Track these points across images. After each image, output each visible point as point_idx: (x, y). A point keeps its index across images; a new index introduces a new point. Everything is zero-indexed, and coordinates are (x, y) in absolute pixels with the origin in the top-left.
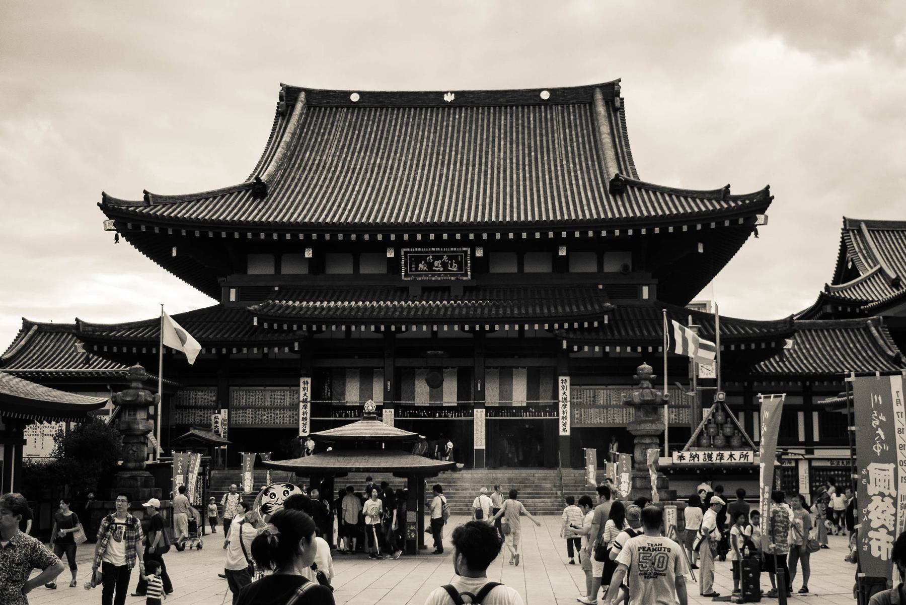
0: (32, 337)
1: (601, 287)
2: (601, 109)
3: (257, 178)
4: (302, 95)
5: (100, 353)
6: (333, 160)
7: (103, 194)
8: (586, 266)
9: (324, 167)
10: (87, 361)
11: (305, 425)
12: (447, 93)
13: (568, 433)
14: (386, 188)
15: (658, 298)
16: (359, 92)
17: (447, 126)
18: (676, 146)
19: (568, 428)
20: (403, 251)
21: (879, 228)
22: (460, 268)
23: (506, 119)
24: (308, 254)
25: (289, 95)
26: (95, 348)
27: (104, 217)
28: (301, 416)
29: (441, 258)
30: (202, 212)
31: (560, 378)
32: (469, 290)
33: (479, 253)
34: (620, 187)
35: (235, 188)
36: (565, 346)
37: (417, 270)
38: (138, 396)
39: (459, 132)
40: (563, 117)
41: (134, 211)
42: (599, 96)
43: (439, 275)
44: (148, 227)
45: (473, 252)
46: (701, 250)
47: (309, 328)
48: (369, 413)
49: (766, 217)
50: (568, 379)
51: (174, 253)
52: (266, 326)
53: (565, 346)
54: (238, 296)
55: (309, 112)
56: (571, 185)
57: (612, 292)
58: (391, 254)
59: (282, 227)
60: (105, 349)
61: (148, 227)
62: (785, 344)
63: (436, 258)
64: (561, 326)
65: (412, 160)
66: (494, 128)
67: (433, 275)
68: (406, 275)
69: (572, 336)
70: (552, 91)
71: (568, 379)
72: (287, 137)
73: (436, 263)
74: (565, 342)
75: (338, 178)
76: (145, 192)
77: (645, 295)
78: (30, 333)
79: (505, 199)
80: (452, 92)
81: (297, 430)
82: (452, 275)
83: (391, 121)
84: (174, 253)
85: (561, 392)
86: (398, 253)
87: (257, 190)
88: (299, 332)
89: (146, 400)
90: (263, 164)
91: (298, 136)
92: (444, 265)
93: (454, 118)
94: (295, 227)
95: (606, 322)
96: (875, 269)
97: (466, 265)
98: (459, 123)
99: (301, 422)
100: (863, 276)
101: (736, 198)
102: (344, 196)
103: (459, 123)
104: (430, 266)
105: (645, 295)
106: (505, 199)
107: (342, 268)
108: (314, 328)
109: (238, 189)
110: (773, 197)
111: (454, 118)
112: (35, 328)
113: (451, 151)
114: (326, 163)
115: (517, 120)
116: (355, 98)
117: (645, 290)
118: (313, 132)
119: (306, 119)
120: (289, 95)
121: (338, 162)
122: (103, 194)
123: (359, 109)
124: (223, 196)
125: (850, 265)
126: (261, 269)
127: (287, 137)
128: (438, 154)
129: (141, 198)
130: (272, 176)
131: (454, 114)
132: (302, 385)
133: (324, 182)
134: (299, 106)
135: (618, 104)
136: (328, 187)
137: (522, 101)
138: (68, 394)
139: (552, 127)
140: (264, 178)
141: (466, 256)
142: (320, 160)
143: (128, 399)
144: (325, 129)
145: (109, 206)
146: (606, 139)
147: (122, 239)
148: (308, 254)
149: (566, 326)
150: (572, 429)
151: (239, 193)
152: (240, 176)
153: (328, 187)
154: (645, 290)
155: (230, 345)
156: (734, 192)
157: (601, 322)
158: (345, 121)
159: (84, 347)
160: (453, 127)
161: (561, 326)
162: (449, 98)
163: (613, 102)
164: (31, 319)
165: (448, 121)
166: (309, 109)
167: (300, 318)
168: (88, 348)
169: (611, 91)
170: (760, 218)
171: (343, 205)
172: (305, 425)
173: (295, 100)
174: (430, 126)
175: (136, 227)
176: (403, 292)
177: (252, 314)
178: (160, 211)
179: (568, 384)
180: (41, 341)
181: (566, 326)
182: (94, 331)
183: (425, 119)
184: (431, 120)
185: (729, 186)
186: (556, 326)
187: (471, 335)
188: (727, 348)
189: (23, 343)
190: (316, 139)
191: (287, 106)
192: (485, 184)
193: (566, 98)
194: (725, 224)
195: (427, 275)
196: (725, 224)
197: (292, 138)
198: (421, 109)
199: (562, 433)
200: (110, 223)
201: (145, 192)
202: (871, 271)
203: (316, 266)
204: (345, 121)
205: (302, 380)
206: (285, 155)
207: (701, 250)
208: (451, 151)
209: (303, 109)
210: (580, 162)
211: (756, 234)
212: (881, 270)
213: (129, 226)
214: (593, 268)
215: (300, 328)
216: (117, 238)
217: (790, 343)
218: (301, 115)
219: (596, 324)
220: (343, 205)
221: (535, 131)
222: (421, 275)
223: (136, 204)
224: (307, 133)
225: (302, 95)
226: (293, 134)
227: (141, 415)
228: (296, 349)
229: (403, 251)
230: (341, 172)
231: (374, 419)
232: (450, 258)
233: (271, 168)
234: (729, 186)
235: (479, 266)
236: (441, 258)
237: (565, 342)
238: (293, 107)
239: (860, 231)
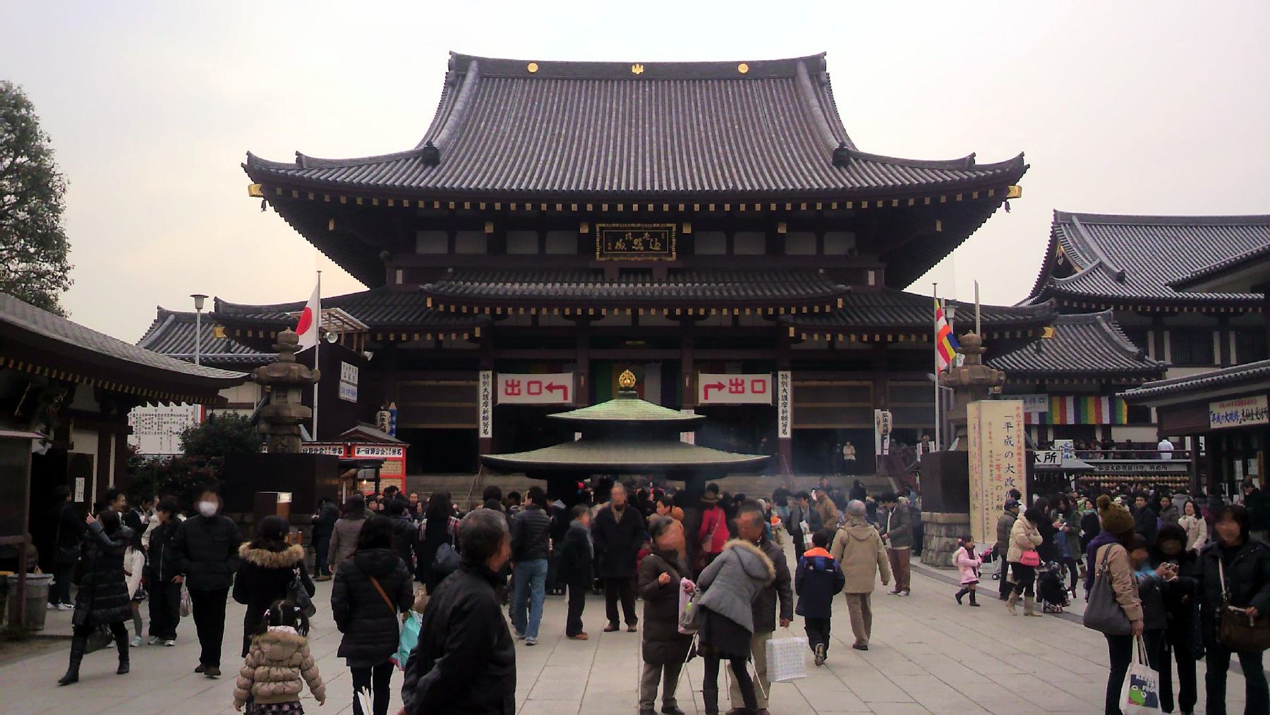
0: (168, 327)
1: (821, 271)
2: (806, 81)
3: (429, 143)
4: (474, 64)
5: (244, 341)
6: (511, 131)
7: (248, 154)
8: (802, 247)
9: (502, 137)
10: (228, 349)
11: (486, 425)
12: (635, 64)
13: (788, 436)
14: (576, 159)
15: (887, 283)
16: (537, 63)
17: (637, 99)
18: (893, 121)
19: (788, 430)
20: (598, 226)
21: (1091, 221)
22: (663, 248)
23: (701, 93)
24: (489, 229)
25: (459, 65)
26: (238, 333)
27: (249, 181)
28: (481, 415)
29: (641, 235)
30: (366, 178)
31: (780, 373)
32: (673, 273)
33: (687, 230)
34: (844, 156)
35: (402, 154)
36: (792, 335)
37: (613, 249)
38: (290, 370)
39: (650, 105)
40: (764, 91)
41: (286, 174)
42: (802, 70)
43: (639, 255)
44: (302, 195)
45: (680, 229)
46: (939, 228)
47: (493, 311)
48: (627, 389)
49: (1020, 188)
50: (789, 373)
51: (331, 227)
52: (441, 308)
53: (792, 335)
54: (405, 279)
55: (478, 82)
56: (787, 158)
57: (837, 274)
58: (584, 230)
59: (460, 195)
60: (250, 334)
61: (302, 195)
62: (1044, 332)
63: (635, 235)
64: (788, 311)
65: (602, 132)
66: (690, 102)
67: (633, 256)
68: (601, 255)
69: (800, 321)
70: (750, 64)
71: (789, 373)
72: (459, 106)
73: (636, 241)
74: (792, 329)
75: (520, 148)
76: (297, 153)
77: (871, 281)
78: (167, 323)
79: (714, 171)
80: (640, 64)
81: (477, 431)
82: (654, 255)
83: (573, 94)
84: (331, 227)
85: (781, 389)
86: (592, 230)
87: (428, 155)
88: (481, 316)
89: (301, 377)
90: (436, 127)
91: (471, 106)
92: (646, 243)
93: (644, 91)
94: (475, 195)
95: (840, 306)
96: (1095, 264)
97: (671, 243)
98: (650, 97)
99: (482, 422)
100: (1080, 272)
101: (983, 168)
102: (529, 165)
103: (650, 97)
104: (629, 244)
105: (871, 281)
106: (714, 171)
107: (523, 245)
108: (499, 311)
109: (406, 156)
110: (1029, 166)
111: (644, 91)
112: (172, 317)
113: (644, 123)
114: (504, 133)
115: (714, 94)
116: (533, 68)
117: (871, 275)
118: (487, 102)
119: (479, 89)
120: (459, 65)
121: (518, 133)
122: (248, 154)
123: (538, 80)
124: (388, 163)
125: (1060, 262)
126: (431, 246)
127: (459, 106)
128: (630, 125)
129: (292, 160)
130: (446, 143)
131: (644, 87)
132: (482, 380)
133: (504, 152)
134: (471, 76)
135: (824, 79)
136: (509, 157)
137: (721, 74)
138: (192, 373)
139: (754, 102)
140: (436, 144)
141: (671, 233)
142: (497, 132)
143: (276, 375)
144: (501, 100)
145: (259, 171)
146: (817, 110)
147: (270, 209)
148: (489, 229)
149: (793, 311)
150: (794, 431)
151: (407, 160)
152: (409, 138)
153: (509, 157)
154: (871, 275)
155: (398, 330)
156: (979, 161)
157: (834, 306)
158: (523, 93)
159: (224, 332)
160: (644, 100)
161: (788, 311)
162: (638, 70)
163: (818, 76)
164: (168, 307)
165: (637, 94)
166: (481, 79)
167: (482, 301)
168: (229, 332)
169: (816, 66)
170: (1013, 190)
171: (529, 174)
172: (486, 425)
173: (466, 69)
174: (618, 99)
175: (287, 193)
176: (598, 274)
177: (425, 294)
178: (315, 174)
179: (789, 380)
180: (179, 332)
181: (793, 311)
182: (236, 314)
183: (612, 92)
184: (618, 93)
185: (974, 155)
186: (782, 311)
187: (571, 323)
188: (990, 335)
189: (158, 333)
190: (491, 110)
191: (458, 76)
192: (688, 155)
193: (764, 72)
194: (969, 195)
195: (625, 255)
196: (969, 195)
197: (465, 108)
198: (606, 82)
199: (781, 435)
200: (256, 188)
201: (297, 153)
202: (1091, 266)
203: (497, 244)
204: (523, 93)
205: (481, 373)
206: (457, 124)
207: (939, 228)
208: (644, 123)
209: (475, 78)
210: (791, 135)
211: (1007, 208)
212: (1101, 264)
213: (279, 191)
214: (811, 250)
215: (482, 311)
216: (264, 207)
217: (1049, 331)
218: (474, 84)
219: (828, 309)
220: (529, 174)
221: (735, 104)
222: (618, 255)
223: (287, 167)
224: (480, 104)
225: (474, 64)
226: (466, 104)
227: (295, 398)
228: (477, 335)
229: (598, 226)
230: (522, 142)
231: (633, 397)
232: (652, 235)
233: (444, 134)
234: (974, 155)
235: (685, 245)
236: (641, 235)
237: (792, 329)
238: (464, 77)
239: (1072, 224)
